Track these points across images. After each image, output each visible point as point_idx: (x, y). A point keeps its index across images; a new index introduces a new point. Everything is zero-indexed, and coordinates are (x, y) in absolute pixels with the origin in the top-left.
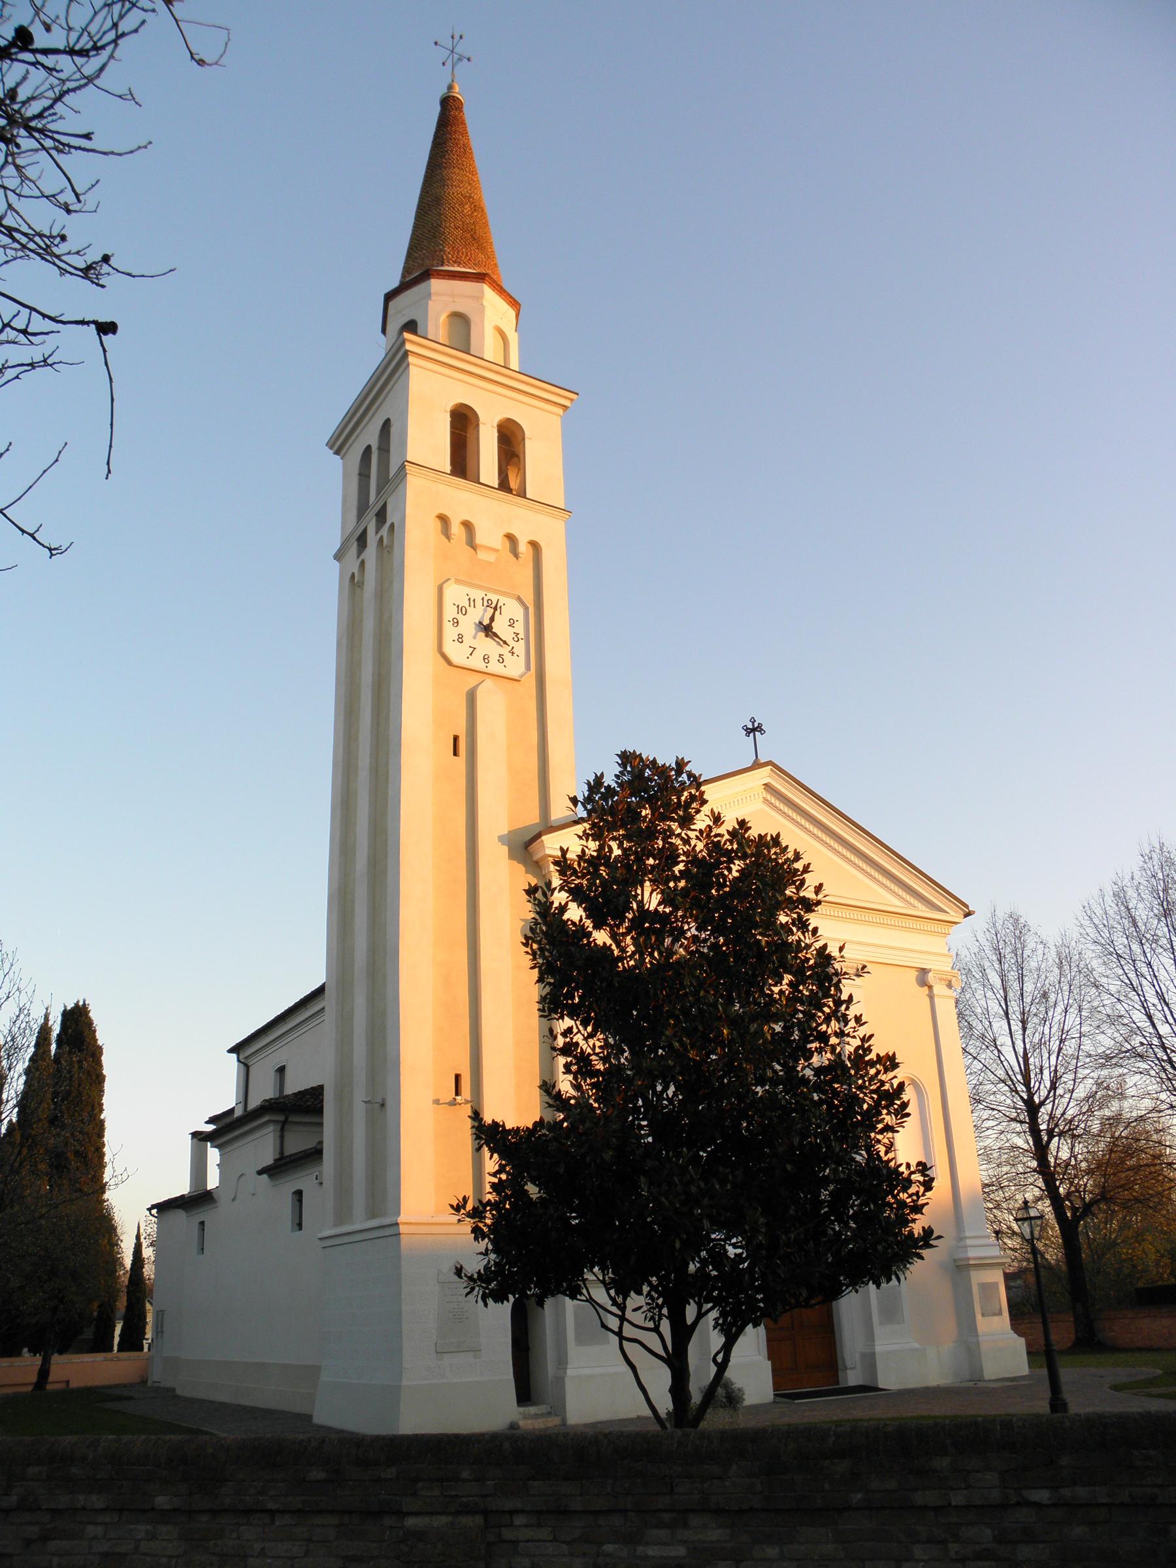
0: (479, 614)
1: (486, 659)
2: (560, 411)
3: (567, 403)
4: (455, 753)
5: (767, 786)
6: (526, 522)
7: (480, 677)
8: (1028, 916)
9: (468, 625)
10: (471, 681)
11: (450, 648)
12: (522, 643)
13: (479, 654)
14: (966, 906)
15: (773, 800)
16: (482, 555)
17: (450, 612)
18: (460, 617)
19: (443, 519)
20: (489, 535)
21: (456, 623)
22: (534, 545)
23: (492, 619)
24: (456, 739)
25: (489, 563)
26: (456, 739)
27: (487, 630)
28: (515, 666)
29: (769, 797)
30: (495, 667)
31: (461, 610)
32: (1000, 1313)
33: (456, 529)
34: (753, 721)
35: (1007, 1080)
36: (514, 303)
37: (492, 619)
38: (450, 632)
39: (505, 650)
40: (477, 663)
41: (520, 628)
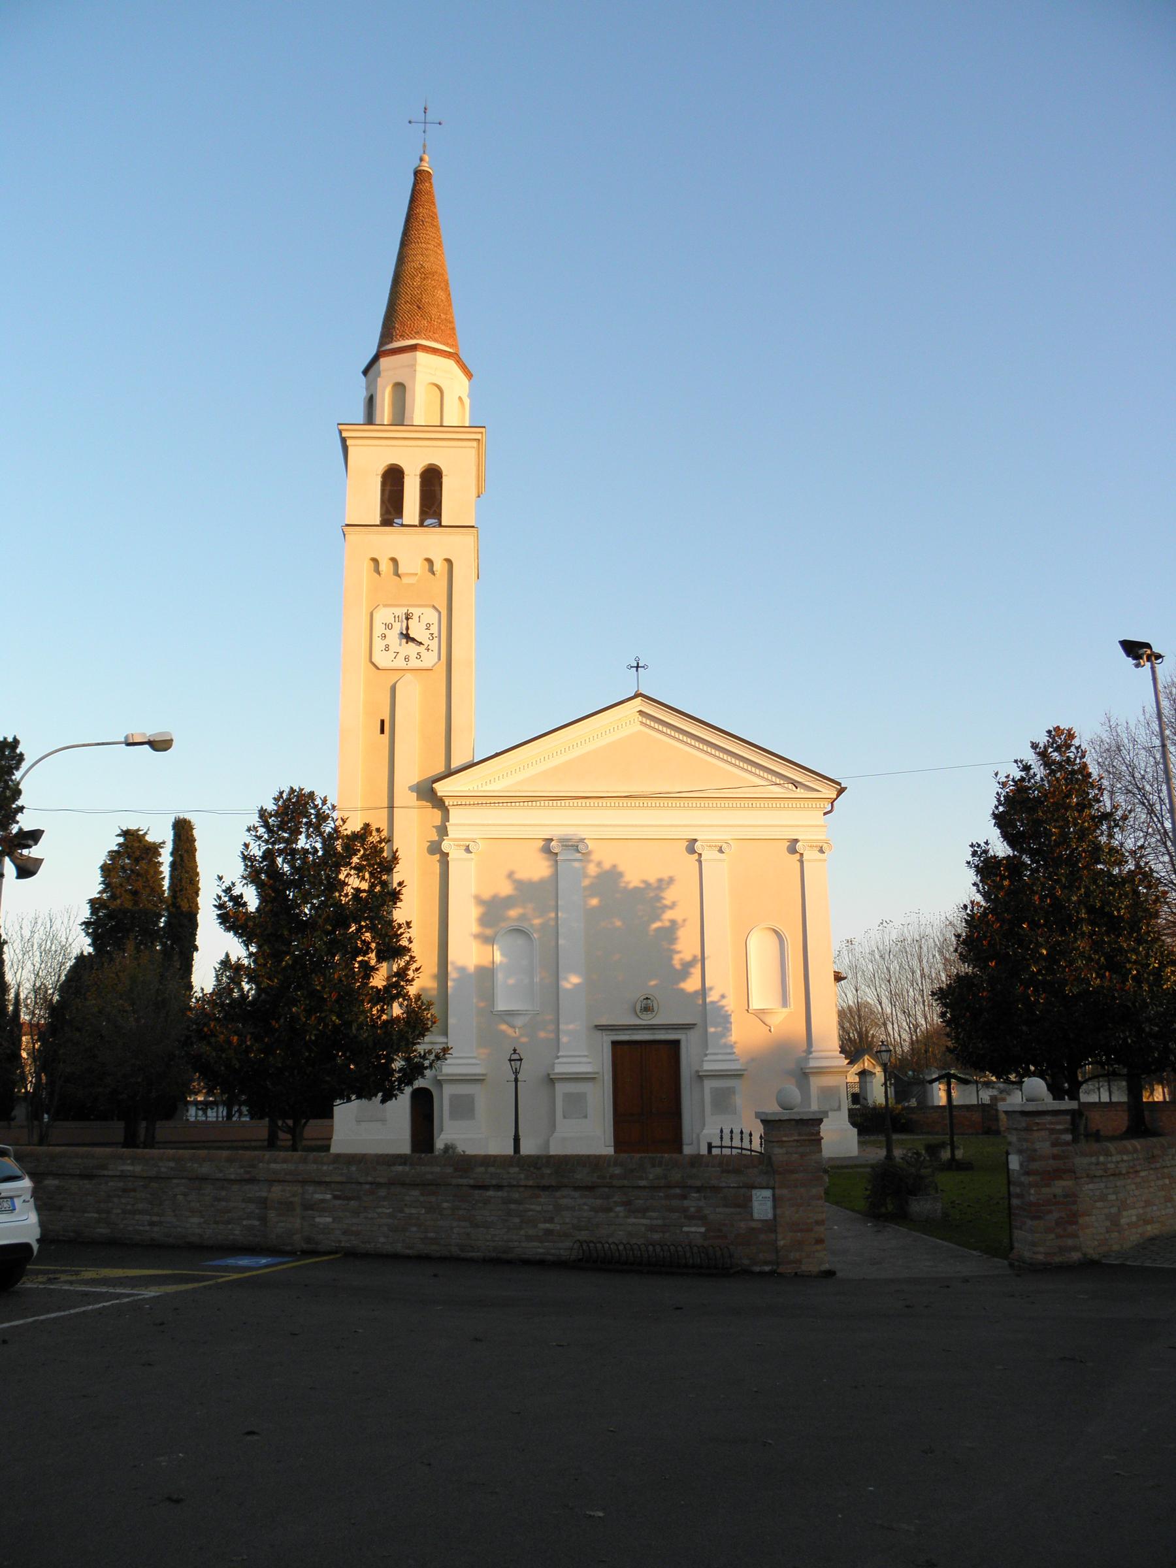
0: (398, 627)
1: (407, 659)
2: (475, 444)
3: (478, 436)
4: (382, 732)
5: (640, 712)
6: (435, 544)
7: (400, 673)
8: (645, 878)
9: (393, 636)
10: (394, 677)
11: (381, 659)
12: (436, 640)
13: (401, 657)
14: (839, 784)
15: (648, 722)
16: (405, 580)
17: (379, 629)
18: (387, 632)
19: (375, 561)
20: (411, 565)
21: (384, 636)
22: (449, 561)
23: (407, 628)
24: (382, 722)
25: (412, 584)
26: (382, 722)
27: (407, 637)
28: (429, 659)
29: (644, 720)
30: (414, 663)
31: (388, 626)
32: (839, 1109)
33: (385, 566)
34: (637, 660)
35: (1149, 750)
36: (469, 374)
37: (407, 628)
38: (378, 644)
39: (422, 649)
40: (400, 663)
41: (434, 629)
